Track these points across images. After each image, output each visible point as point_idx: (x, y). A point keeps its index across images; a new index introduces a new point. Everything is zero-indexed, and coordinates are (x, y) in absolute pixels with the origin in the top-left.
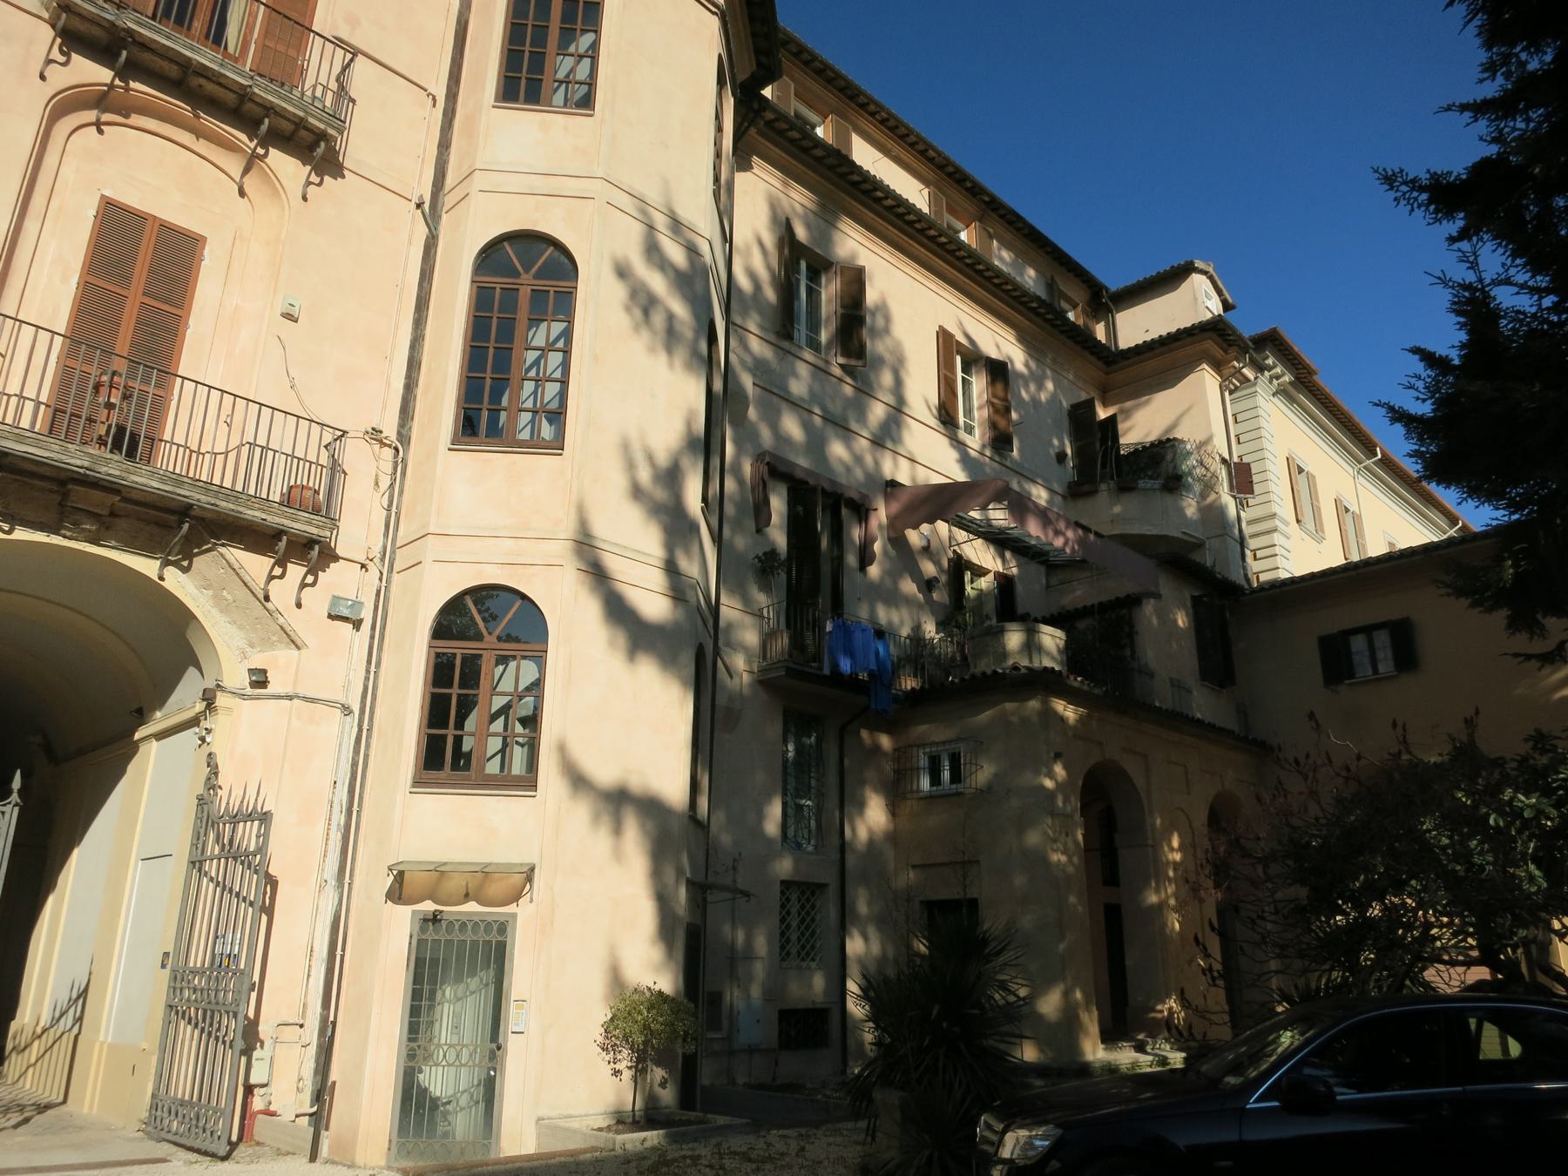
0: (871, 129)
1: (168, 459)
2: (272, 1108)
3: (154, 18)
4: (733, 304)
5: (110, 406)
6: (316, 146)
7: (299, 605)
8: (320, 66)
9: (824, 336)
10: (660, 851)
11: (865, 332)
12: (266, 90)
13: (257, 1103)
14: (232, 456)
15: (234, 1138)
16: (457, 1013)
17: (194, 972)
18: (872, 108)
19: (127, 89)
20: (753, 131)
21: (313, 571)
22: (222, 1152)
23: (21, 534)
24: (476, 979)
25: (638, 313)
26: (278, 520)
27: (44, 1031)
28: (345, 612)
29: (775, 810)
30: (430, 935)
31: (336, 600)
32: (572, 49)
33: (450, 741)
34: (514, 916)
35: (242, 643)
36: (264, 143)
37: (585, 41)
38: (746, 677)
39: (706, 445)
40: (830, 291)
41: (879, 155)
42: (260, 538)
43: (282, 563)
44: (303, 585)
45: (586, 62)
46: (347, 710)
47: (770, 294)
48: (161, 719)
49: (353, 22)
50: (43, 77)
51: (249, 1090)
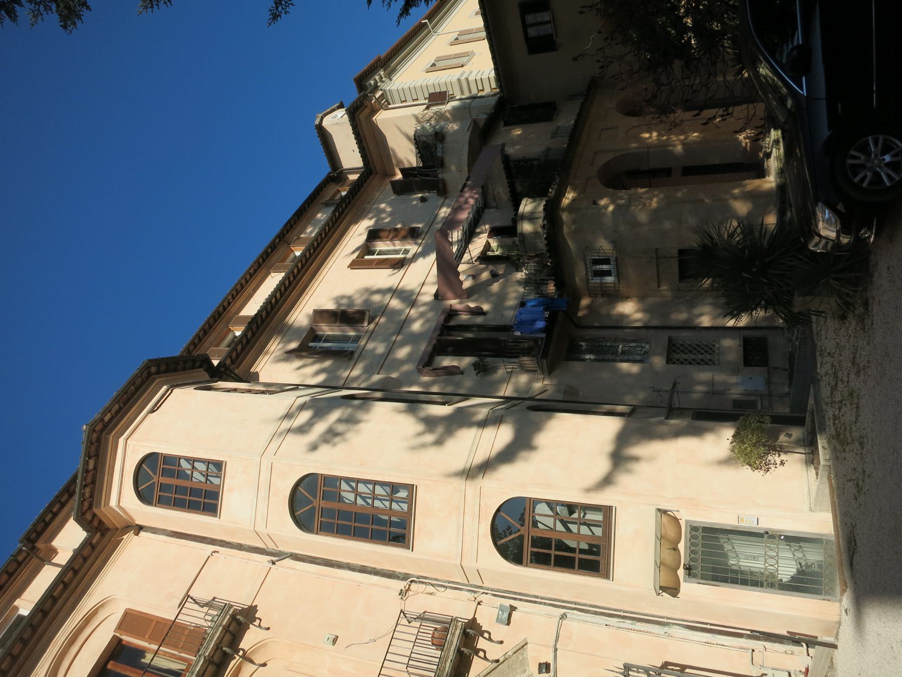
0: (238, 304)
2: (804, 670)
4: (333, 385)
6: (238, 621)
7: (501, 642)
8: (195, 617)
9: (352, 333)
10: (649, 435)
11: (350, 310)
12: (207, 648)
16: (747, 558)
18: (226, 304)
20: (236, 371)
24: (725, 545)
25: (337, 439)
26: (451, 653)
28: (506, 615)
29: (625, 366)
30: (698, 571)
31: (498, 620)
32: (189, 472)
34: (687, 522)
37: (185, 465)
39: (412, 402)
40: (327, 329)
43: (477, 652)
44: (490, 639)
45: (196, 464)
46: (563, 617)
47: (328, 363)
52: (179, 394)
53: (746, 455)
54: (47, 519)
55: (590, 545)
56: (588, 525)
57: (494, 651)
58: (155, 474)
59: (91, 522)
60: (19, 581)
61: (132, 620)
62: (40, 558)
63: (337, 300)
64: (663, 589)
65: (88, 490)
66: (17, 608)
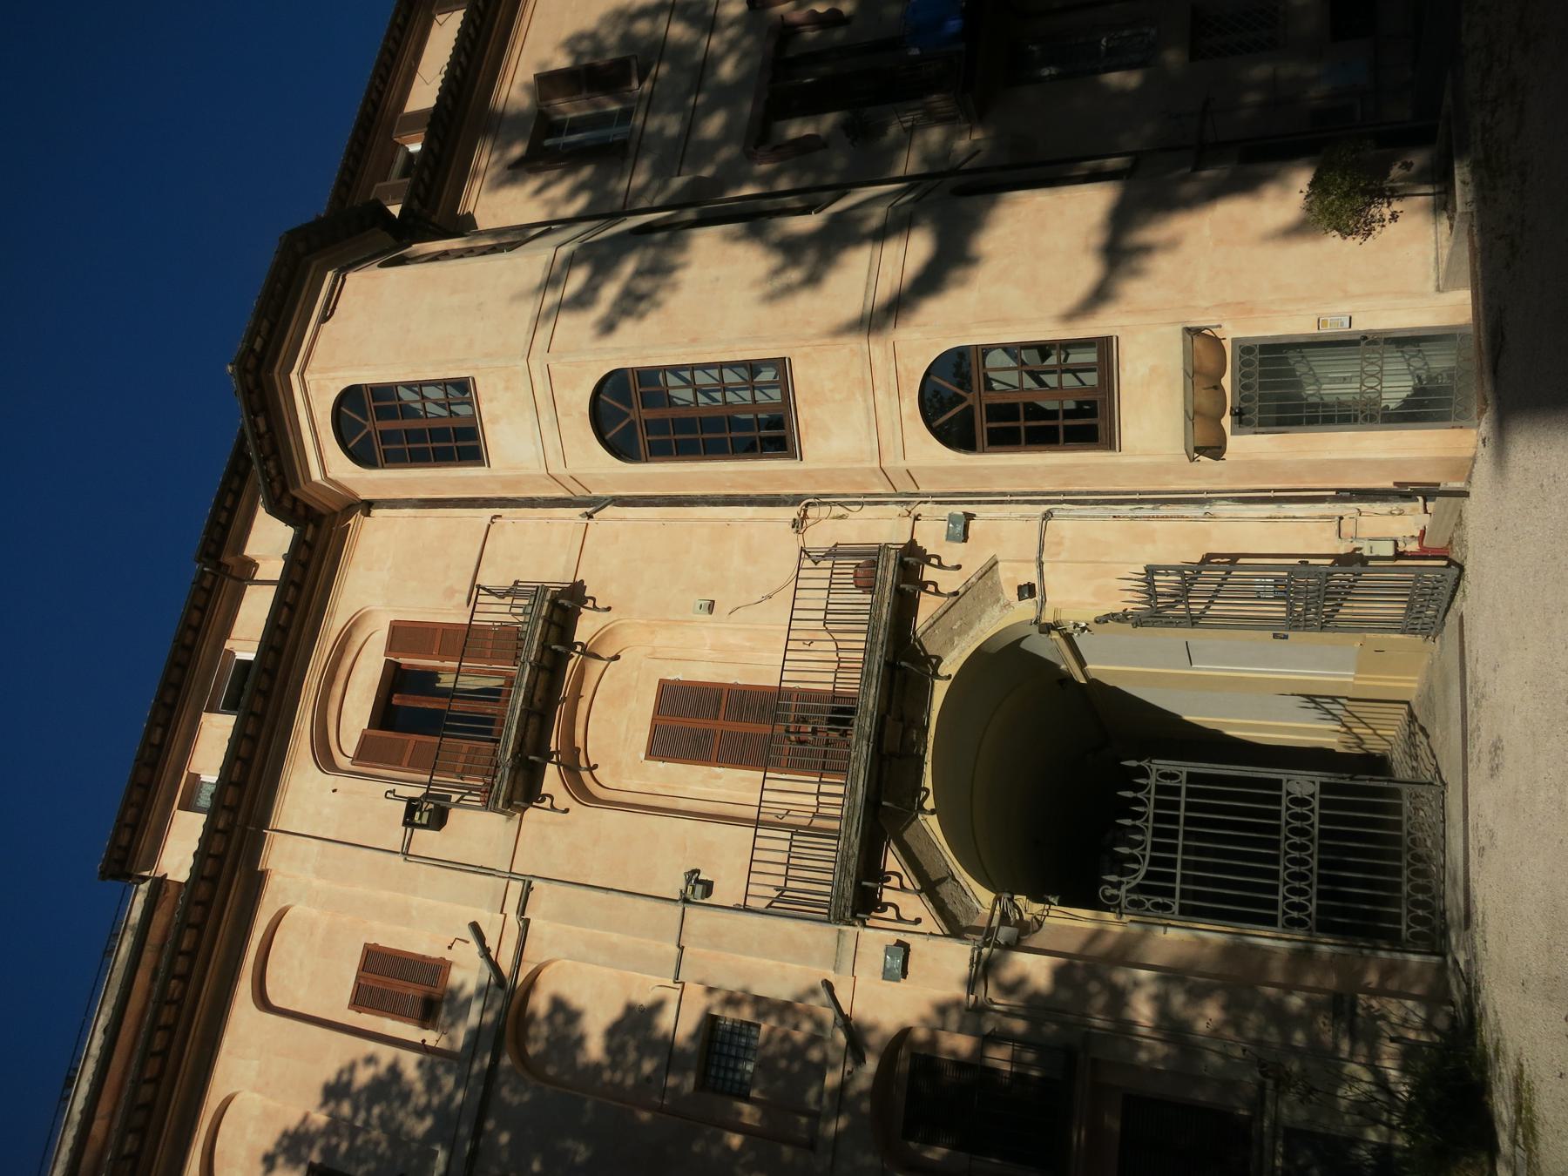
0: (395, 93)
1: (850, 683)
2: (1417, 534)
3: (498, 741)
4: (606, 210)
5: (814, 731)
6: (564, 605)
7: (958, 567)
8: (495, 613)
9: (614, 107)
10: (1168, 202)
11: (600, 62)
12: (530, 651)
13: (1413, 547)
14: (837, 636)
15: (1444, 563)
16: (1335, 382)
17: (1290, 611)
18: (374, 96)
19: (557, 752)
20: (435, 219)
21: (925, 558)
22: (1454, 571)
23: (928, 782)
24: (1297, 366)
25: (643, 306)
26: (887, 594)
27: (1344, 725)
28: (960, 528)
29: (1114, 78)
30: (1255, 416)
31: (950, 537)
32: (418, 406)
33: (1069, 422)
34: (1234, 341)
35: (997, 609)
36: (573, 646)
37: (406, 395)
38: (977, 135)
39: (752, 220)
40: (567, 108)
41: (418, 78)
42: (905, 606)
43: (923, 586)
44: (940, 566)
45: (427, 391)
46: (1047, 516)
47: (586, 172)
48: (1069, 665)
49: (450, 593)
50: (567, 811)
51: (1399, 555)
52: (356, 280)
53: (1332, 213)
54: (223, 520)
55: (1079, 403)
56: (1074, 371)
57: (949, 582)
58: (366, 419)
59: (294, 510)
60: (218, 617)
61: (403, 635)
62: (235, 578)
63: (572, 44)
64: (1200, 450)
65: (271, 464)
66: (231, 653)
